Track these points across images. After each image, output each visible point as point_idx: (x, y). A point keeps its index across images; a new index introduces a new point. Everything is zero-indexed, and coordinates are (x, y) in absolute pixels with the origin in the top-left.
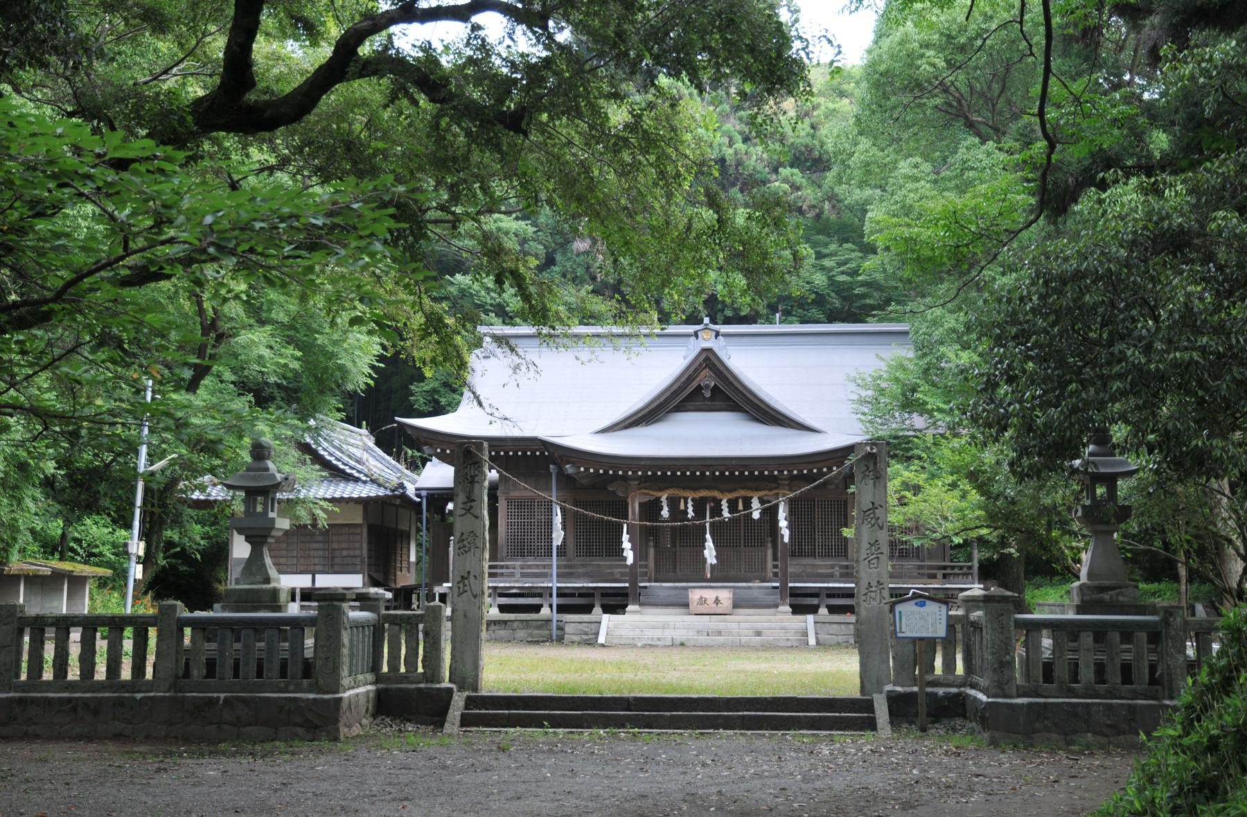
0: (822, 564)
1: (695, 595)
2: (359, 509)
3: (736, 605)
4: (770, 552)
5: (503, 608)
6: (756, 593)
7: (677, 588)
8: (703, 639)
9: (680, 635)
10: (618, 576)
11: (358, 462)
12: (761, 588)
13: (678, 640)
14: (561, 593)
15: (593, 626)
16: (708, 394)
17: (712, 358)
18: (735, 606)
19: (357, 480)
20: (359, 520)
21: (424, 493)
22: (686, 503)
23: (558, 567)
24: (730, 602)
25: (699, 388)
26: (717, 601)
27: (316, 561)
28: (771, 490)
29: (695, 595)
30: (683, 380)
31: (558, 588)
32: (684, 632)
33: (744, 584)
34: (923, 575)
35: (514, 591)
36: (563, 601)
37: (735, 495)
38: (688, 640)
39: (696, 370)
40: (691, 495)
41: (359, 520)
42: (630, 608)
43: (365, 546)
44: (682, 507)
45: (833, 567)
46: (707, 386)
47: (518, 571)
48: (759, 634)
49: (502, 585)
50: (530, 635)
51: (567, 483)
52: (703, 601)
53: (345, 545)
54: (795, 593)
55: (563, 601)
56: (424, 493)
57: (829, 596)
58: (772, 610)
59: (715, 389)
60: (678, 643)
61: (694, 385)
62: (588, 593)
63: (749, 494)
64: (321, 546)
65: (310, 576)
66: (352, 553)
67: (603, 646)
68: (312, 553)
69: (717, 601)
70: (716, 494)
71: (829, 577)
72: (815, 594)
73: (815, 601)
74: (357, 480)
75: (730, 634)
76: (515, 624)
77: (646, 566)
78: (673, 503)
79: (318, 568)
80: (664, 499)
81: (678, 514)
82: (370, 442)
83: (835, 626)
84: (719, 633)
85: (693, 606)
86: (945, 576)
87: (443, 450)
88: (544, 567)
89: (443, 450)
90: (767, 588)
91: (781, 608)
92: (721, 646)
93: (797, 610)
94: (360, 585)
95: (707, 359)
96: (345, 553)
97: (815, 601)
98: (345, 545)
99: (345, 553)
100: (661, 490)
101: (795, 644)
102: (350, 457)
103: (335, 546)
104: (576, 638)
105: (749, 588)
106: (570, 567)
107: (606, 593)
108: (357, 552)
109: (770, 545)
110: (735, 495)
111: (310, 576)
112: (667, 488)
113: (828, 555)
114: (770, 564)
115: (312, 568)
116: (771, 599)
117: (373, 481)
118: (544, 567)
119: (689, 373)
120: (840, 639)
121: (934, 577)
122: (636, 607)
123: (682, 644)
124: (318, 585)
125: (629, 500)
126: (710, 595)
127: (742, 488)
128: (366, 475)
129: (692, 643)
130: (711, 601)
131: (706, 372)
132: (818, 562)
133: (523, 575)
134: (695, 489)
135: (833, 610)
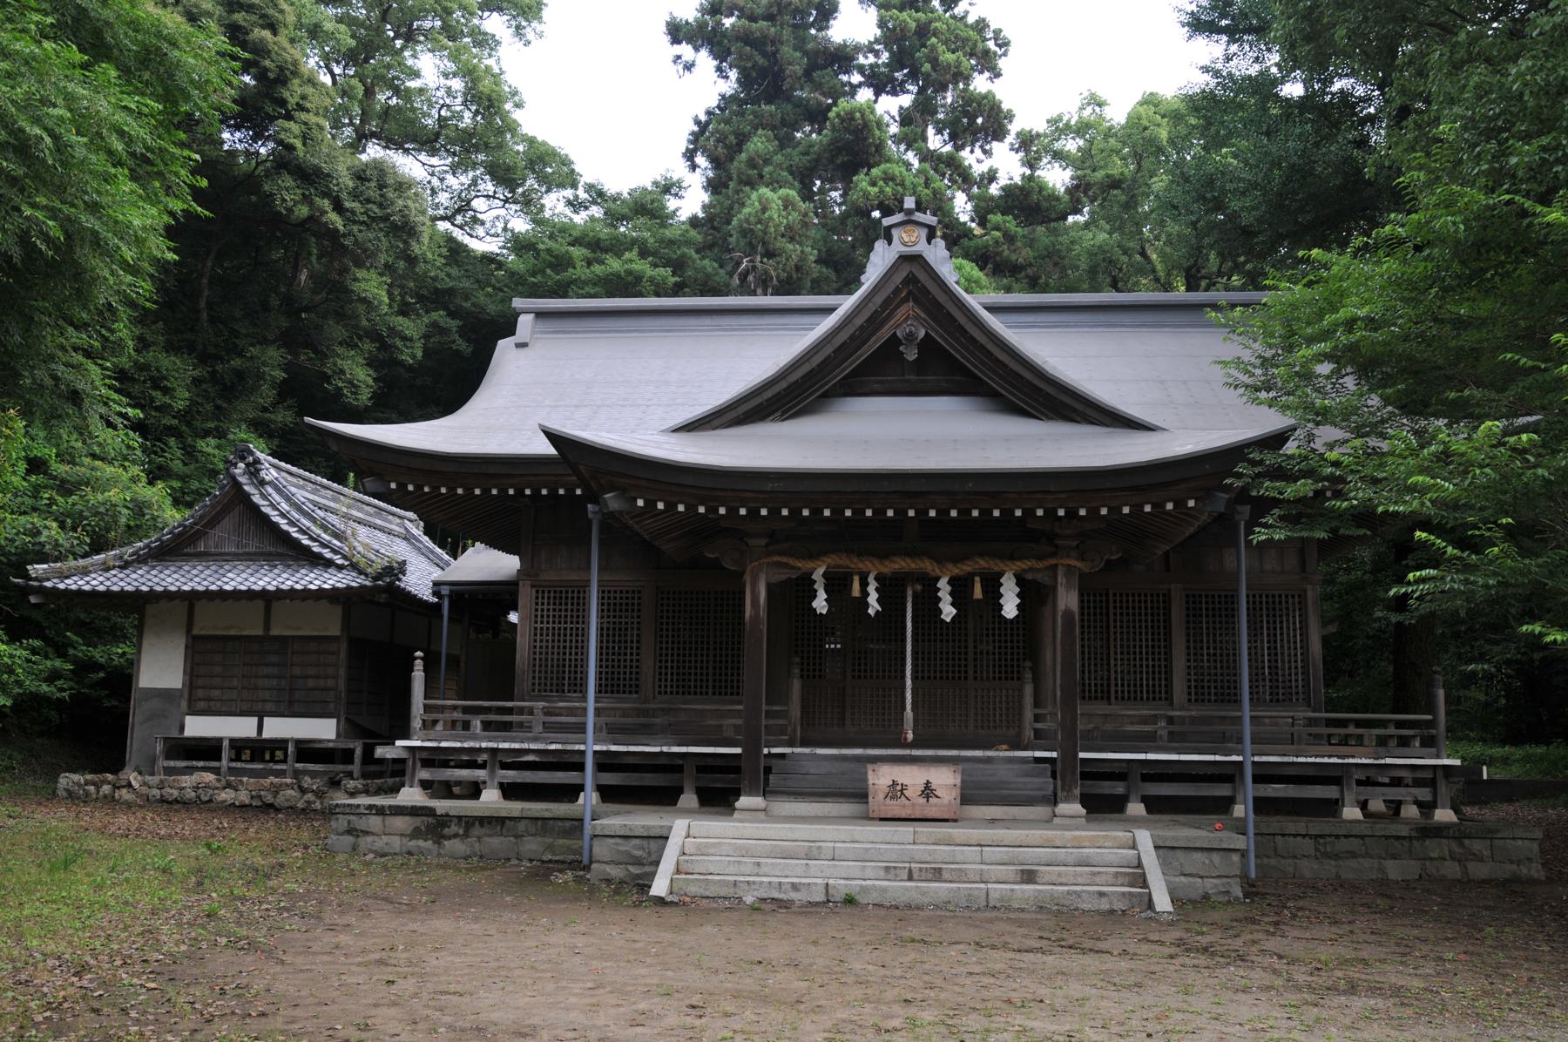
0: (1129, 715)
1: (881, 778)
2: (337, 612)
3: (970, 795)
4: (1028, 690)
5: (509, 791)
6: (1004, 773)
7: (845, 758)
8: (900, 889)
9: (843, 877)
10: (729, 733)
11: (336, 536)
12: (1010, 760)
13: (841, 887)
14: (606, 763)
15: (653, 845)
16: (911, 355)
17: (922, 276)
18: (966, 799)
19: (329, 564)
20: (335, 631)
21: (445, 590)
22: (864, 584)
23: (598, 712)
24: (956, 793)
25: (894, 341)
26: (928, 791)
27: (267, 695)
28: (1040, 558)
29: (881, 778)
30: (859, 321)
31: (595, 752)
32: (852, 867)
33: (978, 753)
34: (1318, 737)
35: (531, 758)
36: (610, 779)
37: (967, 568)
38: (864, 889)
39: (887, 302)
40: (873, 569)
41: (335, 631)
42: (744, 801)
43: (342, 672)
44: (856, 591)
45: (1153, 719)
46: (910, 337)
47: (537, 721)
48: (1029, 877)
49: (506, 745)
50: (550, 848)
51: (621, 538)
52: (897, 791)
53: (311, 671)
54: (1093, 773)
55: (610, 779)
56: (445, 590)
57: (1146, 778)
58: (1040, 811)
59: (927, 345)
60: (838, 896)
61: (884, 334)
62: (672, 765)
63: (994, 565)
64: (275, 671)
65: (255, 720)
66: (322, 683)
67: (660, 901)
68: (262, 682)
69: (928, 791)
70: (928, 566)
71: (1146, 741)
72: (1119, 772)
73: (1119, 788)
74: (329, 564)
75: (961, 876)
76: (522, 826)
77: (784, 714)
78: (837, 584)
79: (269, 706)
80: (818, 575)
81: (846, 603)
82: (417, 531)
83: (1198, 856)
84: (937, 874)
85: (878, 802)
86: (487, 726)
87: (402, 486)
88: (571, 712)
89: (402, 486)
90: (1024, 760)
91: (1063, 808)
92: (943, 911)
93: (1102, 806)
94: (333, 736)
95: (910, 280)
96: (311, 683)
97: (1119, 788)
98: (311, 671)
99: (311, 683)
100: (812, 556)
101: (1119, 905)
102: (325, 528)
103: (297, 671)
104: (615, 872)
105: (989, 760)
106: (645, 713)
107: (706, 765)
108: (330, 683)
109: (1028, 675)
110: (967, 568)
111: (255, 720)
112: (826, 553)
113: (1133, 697)
114: (1029, 714)
115: (259, 706)
116: (1045, 783)
117: (354, 566)
118: (571, 712)
119: (872, 308)
120: (1210, 885)
121: (1404, 742)
122: (756, 801)
123: (850, 901)
124: (266, 735)
125: (747, 578)
126: (912, 777)
127: (982, 555)
128: (345, 557)
129: (873, 898)
130: (913, 792)
131: (909, 308)
132: (1115, 709)
133: (548, 727)
134: (883, 556)
135: (1155, 806)
